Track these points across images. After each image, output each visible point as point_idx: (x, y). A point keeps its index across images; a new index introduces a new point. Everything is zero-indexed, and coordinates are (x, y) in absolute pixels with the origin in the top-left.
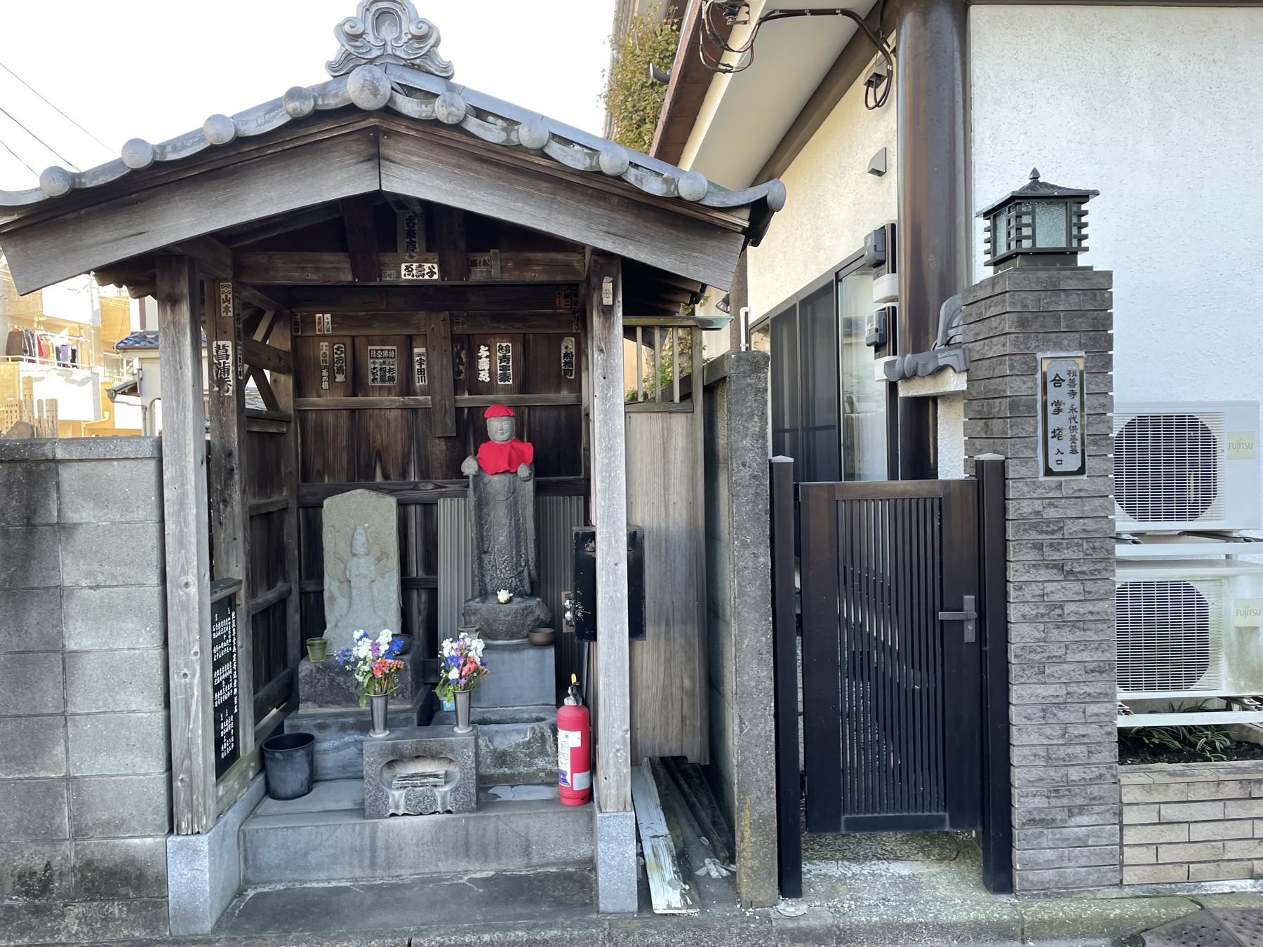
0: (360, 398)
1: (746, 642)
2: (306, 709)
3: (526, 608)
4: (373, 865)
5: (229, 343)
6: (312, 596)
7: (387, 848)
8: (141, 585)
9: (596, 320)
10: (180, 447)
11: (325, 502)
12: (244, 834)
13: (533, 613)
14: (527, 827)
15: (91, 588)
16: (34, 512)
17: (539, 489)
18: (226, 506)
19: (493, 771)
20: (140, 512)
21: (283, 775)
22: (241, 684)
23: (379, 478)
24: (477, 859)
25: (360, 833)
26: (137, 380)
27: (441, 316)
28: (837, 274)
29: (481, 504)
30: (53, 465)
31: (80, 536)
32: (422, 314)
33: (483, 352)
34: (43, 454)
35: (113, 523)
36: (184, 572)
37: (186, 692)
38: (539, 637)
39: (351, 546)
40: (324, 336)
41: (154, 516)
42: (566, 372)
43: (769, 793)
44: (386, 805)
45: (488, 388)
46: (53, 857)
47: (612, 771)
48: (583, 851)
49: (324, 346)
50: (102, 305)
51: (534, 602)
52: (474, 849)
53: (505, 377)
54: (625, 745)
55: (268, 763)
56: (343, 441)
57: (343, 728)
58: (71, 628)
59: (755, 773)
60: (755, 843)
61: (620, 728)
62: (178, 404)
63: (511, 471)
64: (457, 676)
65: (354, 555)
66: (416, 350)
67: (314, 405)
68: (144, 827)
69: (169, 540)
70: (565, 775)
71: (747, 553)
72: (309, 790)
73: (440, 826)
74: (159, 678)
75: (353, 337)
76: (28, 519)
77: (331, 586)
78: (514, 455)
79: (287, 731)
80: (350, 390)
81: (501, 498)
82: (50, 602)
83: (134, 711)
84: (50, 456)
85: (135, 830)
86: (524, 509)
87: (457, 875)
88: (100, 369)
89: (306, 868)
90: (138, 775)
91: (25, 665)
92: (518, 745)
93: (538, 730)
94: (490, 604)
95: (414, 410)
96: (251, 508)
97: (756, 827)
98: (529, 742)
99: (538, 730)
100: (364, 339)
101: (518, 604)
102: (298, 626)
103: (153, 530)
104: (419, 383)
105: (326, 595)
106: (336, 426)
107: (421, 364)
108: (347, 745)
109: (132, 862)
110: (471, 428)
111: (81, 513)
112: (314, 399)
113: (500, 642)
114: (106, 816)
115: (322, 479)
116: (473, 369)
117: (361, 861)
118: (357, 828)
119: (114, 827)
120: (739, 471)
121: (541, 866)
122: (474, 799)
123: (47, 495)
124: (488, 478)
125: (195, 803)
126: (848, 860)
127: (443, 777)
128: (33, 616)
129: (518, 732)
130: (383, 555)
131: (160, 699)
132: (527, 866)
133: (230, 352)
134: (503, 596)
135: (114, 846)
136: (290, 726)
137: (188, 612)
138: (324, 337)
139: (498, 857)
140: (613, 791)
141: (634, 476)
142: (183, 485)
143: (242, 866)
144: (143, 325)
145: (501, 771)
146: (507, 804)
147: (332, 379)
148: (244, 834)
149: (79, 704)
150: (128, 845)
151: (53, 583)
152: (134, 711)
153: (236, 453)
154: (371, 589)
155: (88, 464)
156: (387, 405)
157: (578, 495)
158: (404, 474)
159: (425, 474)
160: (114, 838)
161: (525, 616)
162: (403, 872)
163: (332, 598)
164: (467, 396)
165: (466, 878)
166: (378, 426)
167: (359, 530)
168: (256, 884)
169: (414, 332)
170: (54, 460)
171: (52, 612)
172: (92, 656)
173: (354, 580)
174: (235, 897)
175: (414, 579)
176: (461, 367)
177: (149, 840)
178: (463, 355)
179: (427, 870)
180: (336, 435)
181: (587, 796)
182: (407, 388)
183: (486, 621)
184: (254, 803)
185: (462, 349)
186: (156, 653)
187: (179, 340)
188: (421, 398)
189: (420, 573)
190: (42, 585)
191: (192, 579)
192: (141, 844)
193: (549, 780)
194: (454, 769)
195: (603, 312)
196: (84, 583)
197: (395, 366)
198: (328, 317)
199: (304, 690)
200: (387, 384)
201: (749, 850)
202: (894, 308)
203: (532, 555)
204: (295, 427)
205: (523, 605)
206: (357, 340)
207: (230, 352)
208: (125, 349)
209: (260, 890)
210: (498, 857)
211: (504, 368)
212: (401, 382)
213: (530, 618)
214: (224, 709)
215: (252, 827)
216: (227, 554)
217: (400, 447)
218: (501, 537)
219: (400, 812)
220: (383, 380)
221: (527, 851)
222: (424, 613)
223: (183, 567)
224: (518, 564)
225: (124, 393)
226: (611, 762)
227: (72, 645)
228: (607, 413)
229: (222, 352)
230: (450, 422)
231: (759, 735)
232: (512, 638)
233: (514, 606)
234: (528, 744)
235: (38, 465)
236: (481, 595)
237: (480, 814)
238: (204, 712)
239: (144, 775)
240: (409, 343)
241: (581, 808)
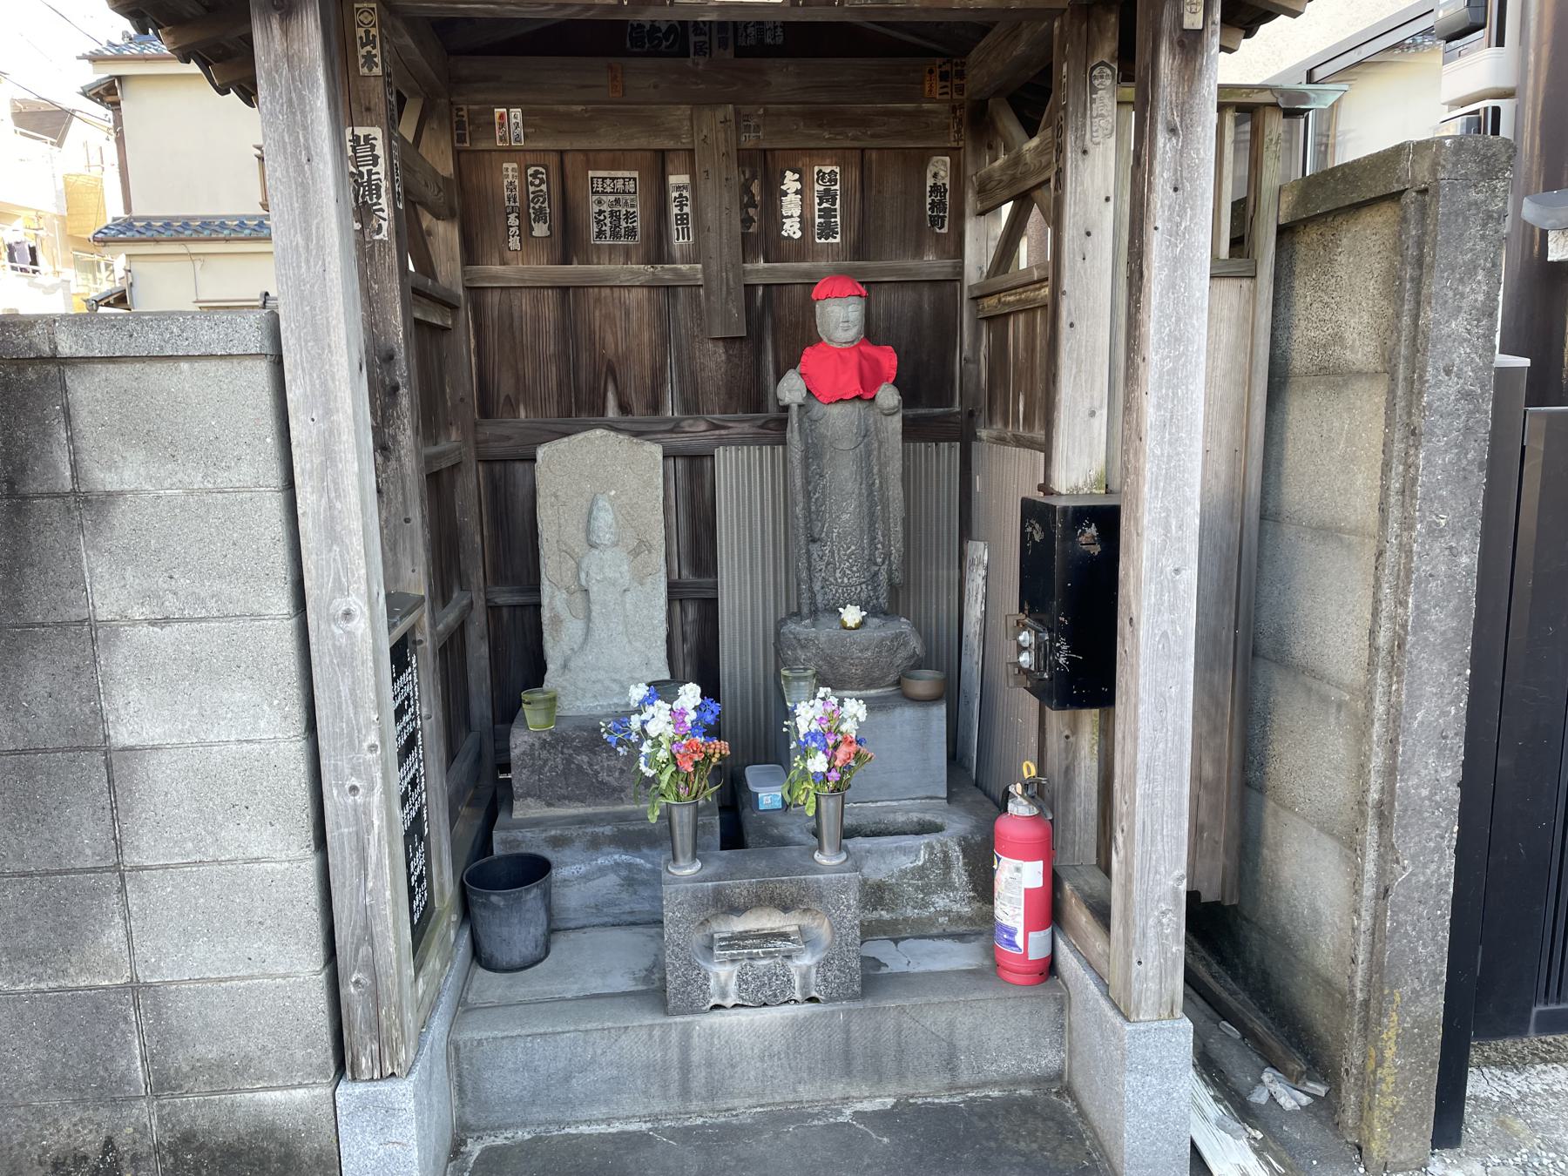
1: (1419, 715)
2: (525, 809)
3: (897, 637)
4: (685, 1093)
5: (377, 132)
6: (505, 612)
7: (709, 1065)
8: (257, 616)
9: (1167, 63)
10: (317, 334)
11: (542, 452)
12: (457, 1049)
13: (905, 644)
14: (951, 1024)
15: (153, 623)
16: (23, 468)
20: (245, 468)
21: (505, 932)
22: (432, 782)
23: (612, 412)
24: (865, 1079)
25: (662, 1040)
26: (126, 286)
27: (720, 115)
28: (1310, 73)
29: (813, 453)
30: (53, 369)
31: (122, 518)
32: (684, 110)
33: (791, 182)
34: (30, 346)
35: (191, 493)
36: (341, 589)
37: (357, 821)
38: (924, 683)
39: (588, 531)
40: (510, 150)
41: (275, 478)
42: (936, 221)
43: (1436, 981)
44: (704, 991)
45: (800, 250)
46: (117, 1128)
47: (1152, 948)
48: (1049, 1060)
49: (510, 168)
50: (67, 185)
51: (904, 625)
52: (858, 1063)
53: (827, 231)
54: (1177, 905)
55: (476, 911)
56: (550, 346)
57: (595, 844)
58: (120, 702)
59: (1414, 950)
60: (1402, 1068)
61: (1168, 873)
62: (308, 239)
63: (866, 397)
64: (823, 768)
65: (593, 546)
66: (673, 180)
67: (495, 278)
68: (289, 1070)
69: (305, 524)
70: (1012, 933)
71: (1437, 548)
72: (547, 952)
73: (800, 1027)
74: (303, 796)
75: (562, 153)
76: (11, 483)
77: (553, 599)
79: (498, 850)
80: (558, 253)
81: (845, 445)
82: (72, 653)
83: (257, 860)
84: (46, 350)
85: (272, 1076)
87: (832, 1107)
88: (69, 273)
89: (567, 1102)
90: (270, 976)
91: (30, 778)
92: (904, 873)
93: (938, 847)
95: (670, 289)
96: (426, 457)
97: (1406, 1042)
99: (938, 847)
100: (581, 157)
101: (880, 630)
102: (485, 663)
103: (274, 504)
104: (679, 241)
105: (546, 614)
107: (681, 206)
108: (602, 871)
109: (271, 1132)
110: (769, 321)
111: (120, 471)
112: (497, 268)
114: (213, 1054)
115: (514, 412)
116: (773, 216)
117: (665, 1087)
118: (657, 1033)
119: (231, 1072)
120: (1438, 384)
121: (973, 1087)
122: (857, 978)
123: (46, 434)
124: (818, 409)
125: (385, 1023)
126: (1495, 1064)
127: (809, 942)
128: (39, 680)
129: (905, 851)
131: (309, 835)
132: (952, 1088)
133: (379, 151)
135: (233, 1107)
136: (504, 842)
137: (353, 669)
138: (509, 152)
139: (901, 1076)
140: (1153, 986)
141: (1151, 402)
142: (328, 412)
143: (455, 1102)
144: (128, 207)
145: (875, 915)
146: (904, 980)
147: (525, 231)
148: (457, 1049)
149: (145, 849)
150: (259, 1104)
151: (73, 614)
152: (257, 860)
153: (401, 355)
154: (623, 603)
155: (127, 368)
156: (624, 279)
157: (950, 440)
158: (655, 406)
159: (691, 406)
160: (233, 1091)
161: (893, 651)
162: (736, 1102)
163: (557, 620)
164: (761, 264)
165: (848, 1112)
167: (600, 501)
168: (479, 1131)
169: (668, 144)
170: (54, 359)
171: (77, 671)
172: (165, 758)
173: (594, 589)
174: (450, 1160)
176: (752, 211)
177: (300, 1094)
178: (755, 188)
179: (778, 1099)
180: (536, 334)
181: (1049, 968)
182: (658, 251)
183: (828, 659)
185: (754, 177)
186: (294, 750)
187: (301, 98)
188: (684, 267)
189: (685, 572)
190: (50, 619)
191: (357, 603)
192: (288, 1100)
193: (953, 929)
194: (821, 928)
195: (1181, 44)
196: (137, 613)
197: (636, 206)
198: (516, 114)
199: (519, 777)
200: (623, 241)
201: (1390, 1079)
202: (1496, 111)
204: (466, 315)
206: (568, 159)
207: (379, 151)
208: (105, 242)
209: (489, 1141)
210: (901, 1076)
211: (827, 214)
212: (647, 237)
213: (902, 654)
214: (415, 833)
215: (467, 1035)
217: (647, 356)
218: (844, 514)
219: (729, 1002)
220: (615, 235)
221: (950, 1063)
223: (337, 580)
225: (108, 305)
226: (1151, 933)
227: (122, 736)
228: (1176, 263)
229: (363, 151)
230: (736, 312)
231: (1427, 884)
232: (868, 687)
234: (921, 872)
235: (20, 371)
237: (869, 1003)
238: (392, 855)
239: (284, 977)
240: (658, 166)
241: (1041, 990)
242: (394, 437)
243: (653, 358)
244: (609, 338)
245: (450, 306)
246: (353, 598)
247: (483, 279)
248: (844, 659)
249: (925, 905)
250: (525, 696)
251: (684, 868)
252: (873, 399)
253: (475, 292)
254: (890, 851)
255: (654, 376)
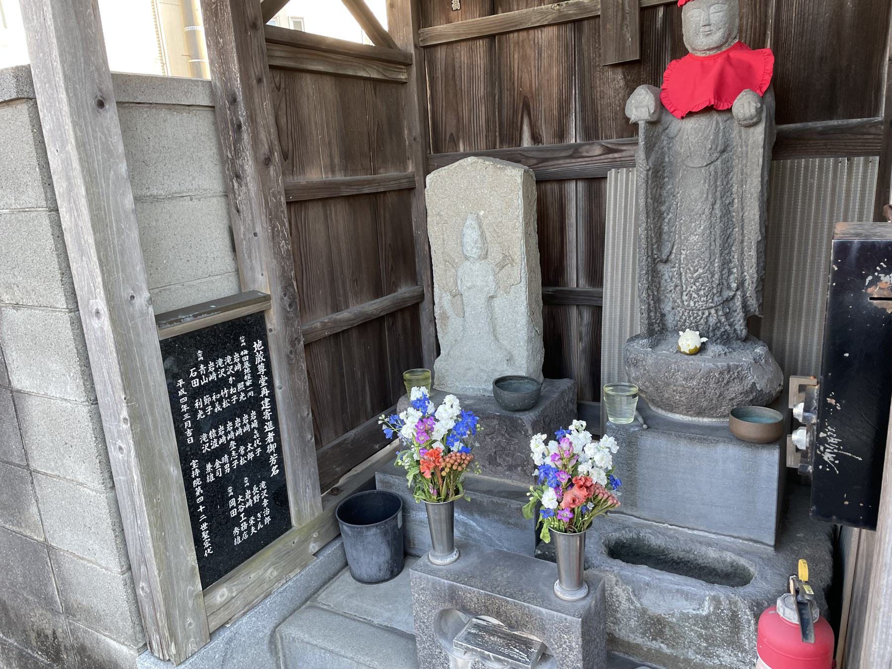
0: (500, 15)
13: (741, 379)
17: (779, 148)
18: (240, 185)
19: (639, 641)
23: (527, 142)
56: (480, 90)
63: (718, 106)
65: (467, 258)
67: (440, 36)
78: (730, 72)
81: (697, 162)
86: (742, 183)
92: (685, 617)
93: (725, 604)
94: (664, 351)
98: (707, 618)
99: (725, 604)
101: (717, 358)
106: (471, 67)
113: (678, 417)
115: (456, 145)
129: (687, 596)
130: (505, 261)
134: (689, 340)
145: (655, 645)
156: (535, 21)
157: (867, 154)
158: (561, 134)
159: (591, 132)
166: (524, 58)
175: (571, 292)
180: (471, 79)
184: (315, 584)
189: (582, 282)
203: (751, 273)
205: (722, 364)
216: (250, 257)
217: (555, 90)
222: (586, 339)
224: (723, 284)
230: (631, 37)
232: (700, 413)
233: (704, 363)
236: (651, 333)
242: (242, 166)
243: (560, 92)
244: (526, 76)
245: (406, 64)
246: (99, 300)
247: (432, 38)
248: (668, 385)
249: (709, 655)
250: (407, 376)
251: (437, 557)
252: (730, 110)
253: (427, 50)
254: (670, 591)
255: (561, 108)
